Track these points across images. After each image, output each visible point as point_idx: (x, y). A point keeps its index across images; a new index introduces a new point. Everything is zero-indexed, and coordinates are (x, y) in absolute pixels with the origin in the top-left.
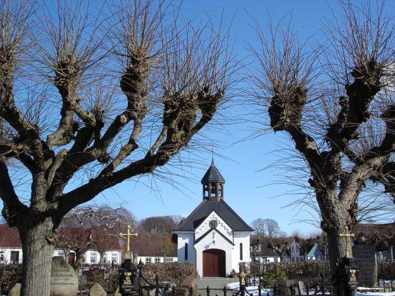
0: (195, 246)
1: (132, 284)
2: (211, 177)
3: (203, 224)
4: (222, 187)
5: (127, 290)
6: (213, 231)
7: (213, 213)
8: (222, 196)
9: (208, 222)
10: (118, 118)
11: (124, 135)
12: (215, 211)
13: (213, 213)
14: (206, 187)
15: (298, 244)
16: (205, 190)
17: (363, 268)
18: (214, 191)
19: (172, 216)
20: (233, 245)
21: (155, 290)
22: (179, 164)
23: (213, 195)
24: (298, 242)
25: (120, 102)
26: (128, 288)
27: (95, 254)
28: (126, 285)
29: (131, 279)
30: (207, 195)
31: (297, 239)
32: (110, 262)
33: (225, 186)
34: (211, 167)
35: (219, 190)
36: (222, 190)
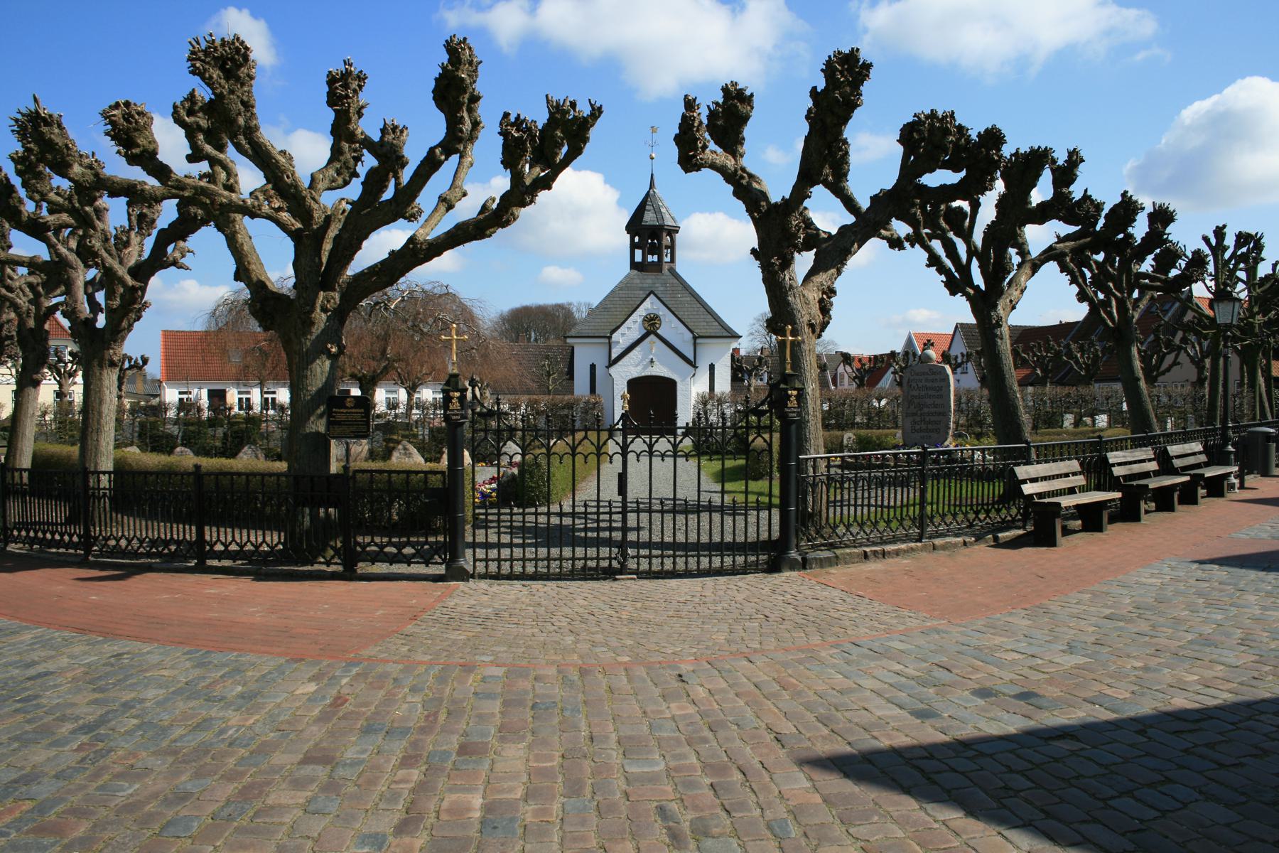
0: (613, 370)
1: (462, 409)
2: (649, 218)
4: (673, 241)
5: (454, 417)
6: (652, 337)
8: (673, 260)
9: (640, 320)
10: (432, 150)
11: (438, 183)
14: (637, 239)
15: (848, 369)
16: (633, 246)
17: (926, 410)
18: (656, 250)
19: (570, 304)
20: (695, 367)
23: (652, 258)
24: (850, 365)
25: (432, 127)
27: (395, 392)
28: (453, 410)
30: (638, 257)
31: (846, 358)
34: (648, 194)
35: (667, 247)
36: (672, 247)
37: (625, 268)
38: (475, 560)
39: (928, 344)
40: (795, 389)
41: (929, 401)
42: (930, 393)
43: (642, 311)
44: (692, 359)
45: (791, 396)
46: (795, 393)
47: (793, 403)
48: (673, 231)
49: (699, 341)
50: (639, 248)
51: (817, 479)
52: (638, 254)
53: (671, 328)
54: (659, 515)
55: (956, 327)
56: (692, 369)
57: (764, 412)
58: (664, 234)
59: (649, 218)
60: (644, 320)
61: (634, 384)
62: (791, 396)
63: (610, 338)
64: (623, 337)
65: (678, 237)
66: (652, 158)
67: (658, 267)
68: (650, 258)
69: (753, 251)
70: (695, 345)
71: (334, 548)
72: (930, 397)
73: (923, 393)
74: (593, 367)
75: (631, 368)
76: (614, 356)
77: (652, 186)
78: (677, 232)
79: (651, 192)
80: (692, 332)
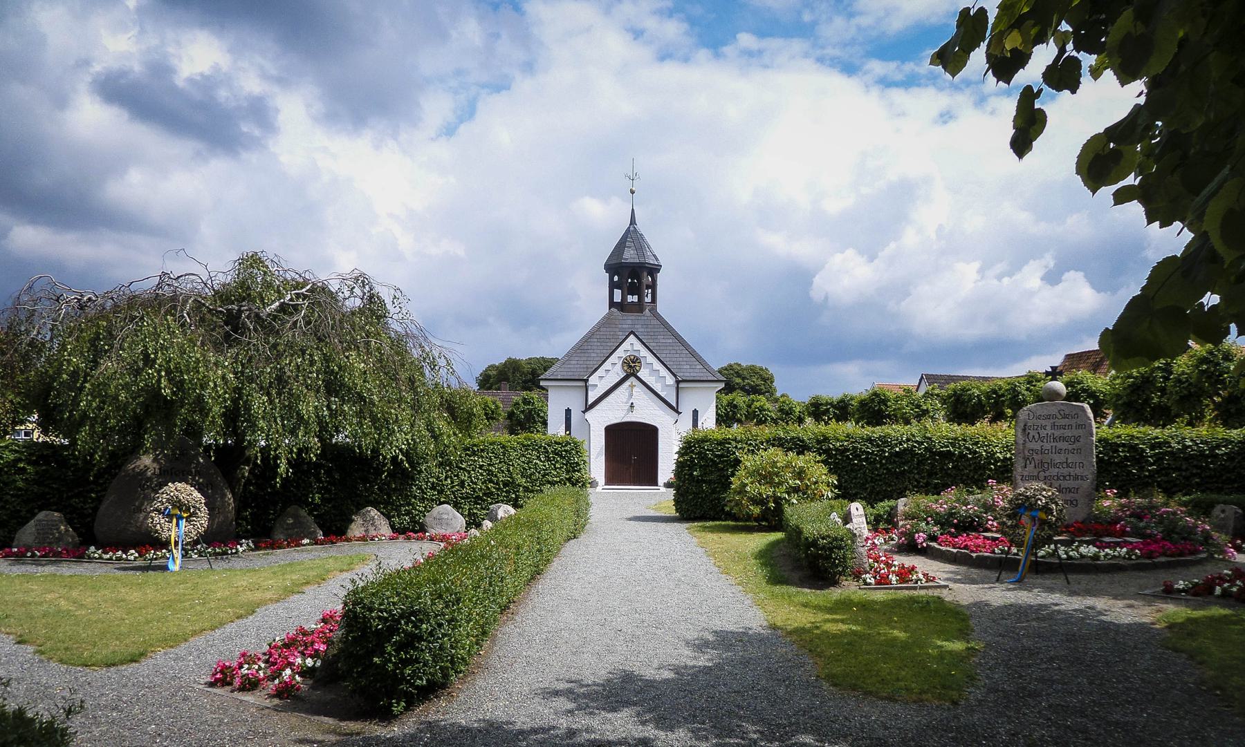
0: (588, 415)
4: (654, 281)
6: (632, 379)
14: (616, 278)
16: (613, 286)
17: (1054, 471)
18: (635, 289)
34: (628, 231)
35: (648, 287)
36: (653, 286)
37: (605, 309)
39: (852, 399)
41: (1058, 459)
42: (1061, 445)
43: (620, 353)
44: (674, 405)
48: (654, 270)
49: (681, 385)
53: (653, 371)
55: (922, 377)
56: (676, 414)
58: (645, 274)
59: (630, 256)
61: (613, 432)
63: (586, 381)
64: (600, 382)
65: (659, 276)
66: (632, 192)
67: (639, 307)
68: (630, 299)
69: (1074, 92)
70: (678, 388)
72: (1059, 451)
73: (1047, 446)
74: (568, 412)
75: (613, 412)
76: (590, 401)
77: (633, 221)
79: (632, 229)
80: (675, 375)
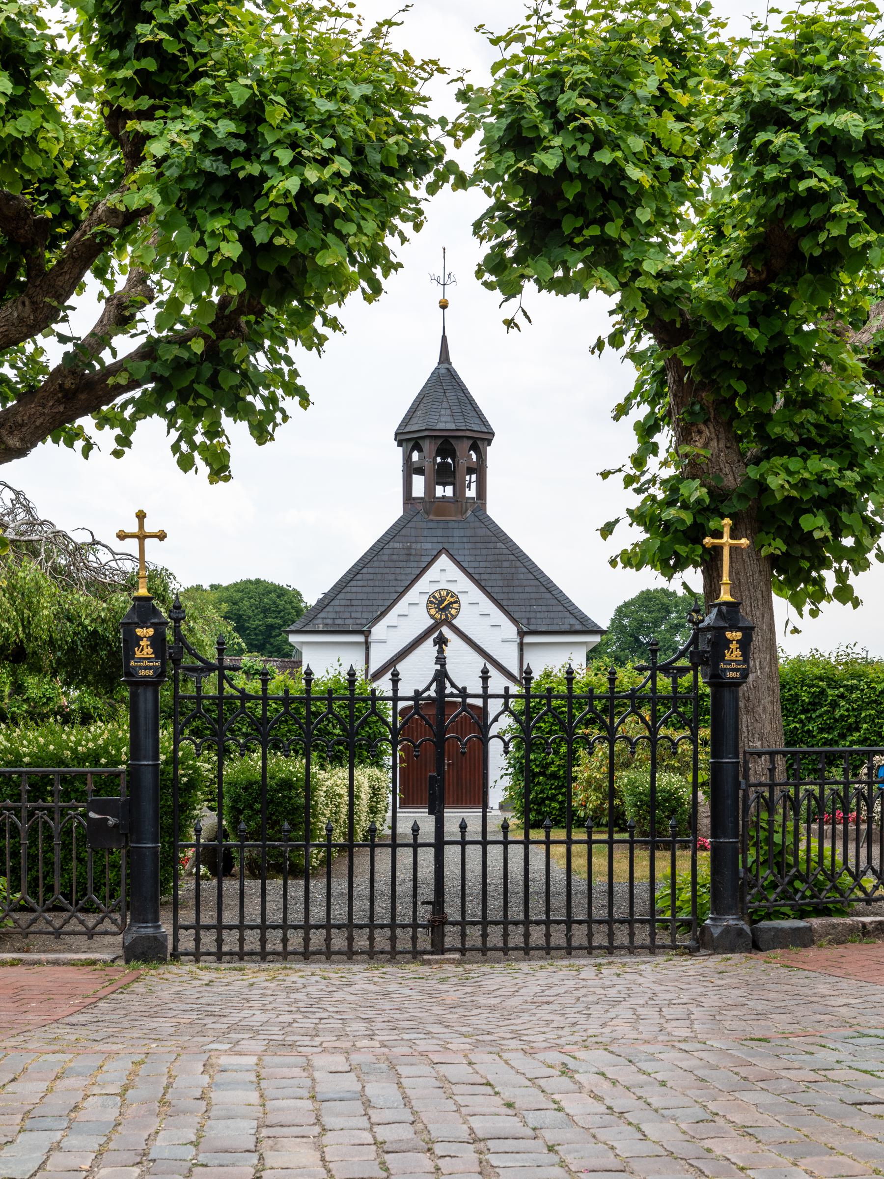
3: (401, 607)
4: (482, 457)
5: (142, 673)
7: (444, 561)
12: (452, 557)
13: (444, 561)
16: (410, 470)
18: (444, 475)
21: (214, 676)
22: (383, 858)
23: (444, 491)
26: (146, 668)
29: (152, 645)
32: (237, 68)
33: (492, 452)
36: (479, 469)
38: (176, 928)
40: (739, 629)
43: (425, 586)
45: (731, 642)
46: (739, 635)
47: (734, 654)
49: (528, 639)
50: (420, 471)
51: (777, 791)
52: (419, 485)
54: (500, 848)
57: (683, 671)
60: (430, 602)
62: (731, 642)
63: (367, 634)
70: (521, 646)
71: (46, 745)
78: (489, 442)
